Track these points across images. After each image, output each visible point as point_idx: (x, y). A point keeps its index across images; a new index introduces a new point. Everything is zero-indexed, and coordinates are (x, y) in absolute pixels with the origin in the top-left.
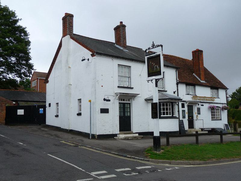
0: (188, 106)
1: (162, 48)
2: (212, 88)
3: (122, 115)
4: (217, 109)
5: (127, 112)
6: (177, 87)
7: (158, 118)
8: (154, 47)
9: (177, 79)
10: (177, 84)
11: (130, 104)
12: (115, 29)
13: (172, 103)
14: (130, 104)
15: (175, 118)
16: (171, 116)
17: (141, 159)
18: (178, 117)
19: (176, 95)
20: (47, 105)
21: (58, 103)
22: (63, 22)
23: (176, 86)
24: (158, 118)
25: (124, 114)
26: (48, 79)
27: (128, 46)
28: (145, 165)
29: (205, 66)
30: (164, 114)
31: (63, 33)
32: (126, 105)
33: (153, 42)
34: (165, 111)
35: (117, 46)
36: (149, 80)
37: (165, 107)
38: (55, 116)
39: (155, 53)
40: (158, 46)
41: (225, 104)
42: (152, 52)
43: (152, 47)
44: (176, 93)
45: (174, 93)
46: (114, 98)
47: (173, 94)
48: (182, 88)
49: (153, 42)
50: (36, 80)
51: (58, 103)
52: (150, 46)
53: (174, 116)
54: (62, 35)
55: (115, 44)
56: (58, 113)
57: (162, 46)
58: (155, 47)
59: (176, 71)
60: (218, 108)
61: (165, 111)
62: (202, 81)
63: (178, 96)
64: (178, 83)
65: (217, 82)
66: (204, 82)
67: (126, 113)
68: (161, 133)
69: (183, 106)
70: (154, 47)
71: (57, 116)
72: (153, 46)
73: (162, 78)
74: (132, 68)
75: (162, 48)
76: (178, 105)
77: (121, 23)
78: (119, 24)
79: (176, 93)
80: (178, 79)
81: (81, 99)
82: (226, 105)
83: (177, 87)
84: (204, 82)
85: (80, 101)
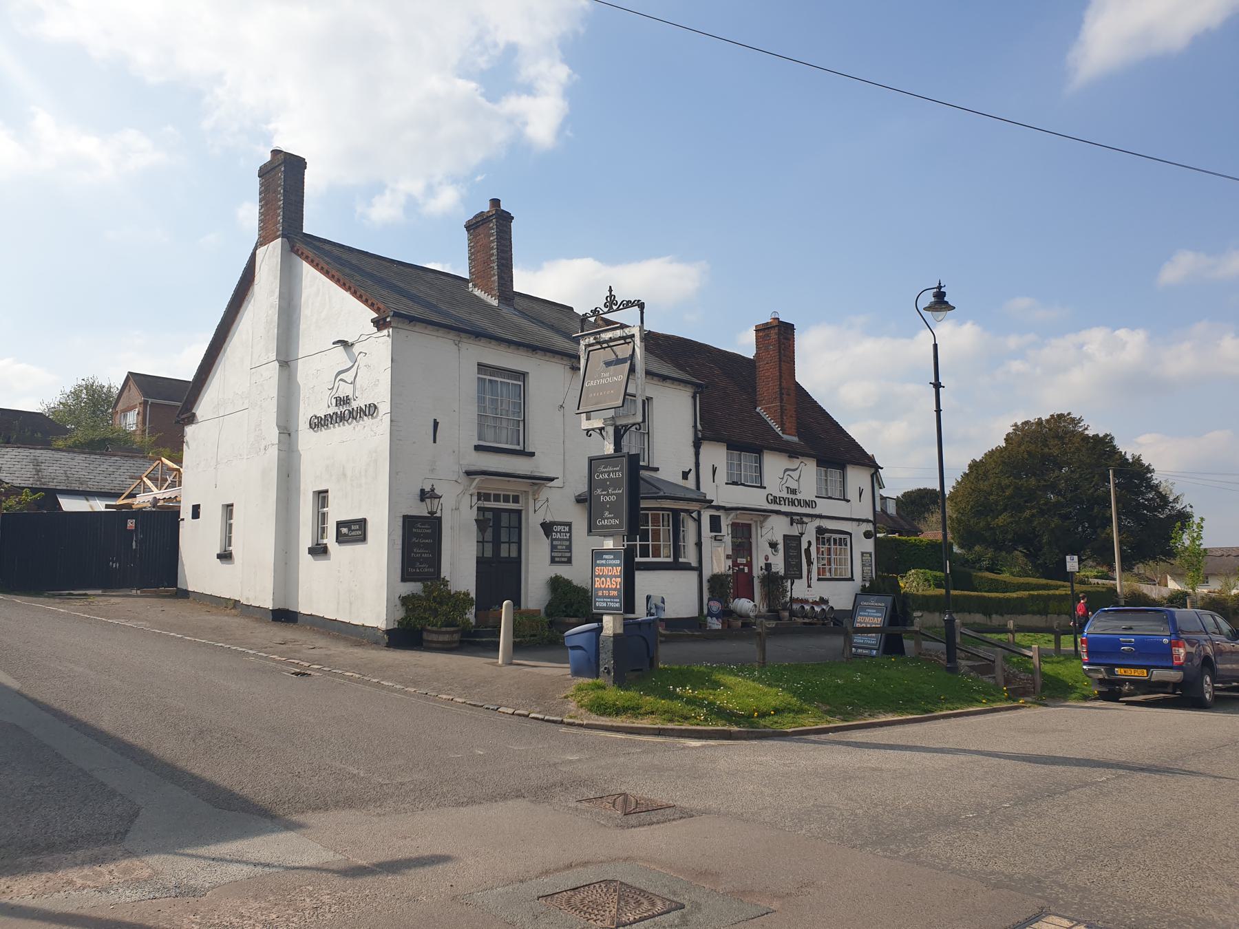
0: (735, 526)
1: (642, 313)
2: (824, 462)
3: (488, 553)
4: (835, 540)
5: (507, 545)
6: (697, 454)
7: (651, 556)
8: (615, 307)
9: (695, 426)
10: (697, 445)
11: (519, 512)
12: (472, 226)
13: (676, 513)
14: (519, 512)
15: (687, 567)
16: (670, 560)
17: (551, 718)
18: (694, 564)
19: (691, 483)
20: (186, 513)
21: (232, 505)
22: (262, 185)
23: (692, 451)
24: (651, 556)
25: (497, 549)
26: (192, 408)
27: (520, 294)
28: (1057, 588)
29: (799, 378)
30: (645, 553)
31: (261, 229)
32: (505, 517)
33: (611, 290)
34: (650, 543)
35: (477, 292)
36: (593, 430)
37: (650, 528)
38: (220, 557)
39: (623, 326)
40: (628, 304)
41: (867, 521)
42: (608, 322)
43: (605, 306)
44: (692, 476)
45: (685, 475)
46: (460, 489)
47: (678, 480)
48: (715, 455)
49: (611, 290)
50: (134, 407)
51: (232, 505)
52: (600, 303)
53: (681, 560)
54: (255, 237)
55: (470, 285)
56: (230, 545)
57: (641, 306)
58: (618, 309)
59: (694, 398)
60: (843, 536)
61: (650, 543)
62: (786, 437)
63: (698, 487)
64: (700, 439)
65: (847, 437)
66: (795, 439)
67: (504, 547)
68: (1023, 424)
69: (715, 524)
70: (615, 307)
71: (225, 556)
72: (611, 302)
73: (639, 424)
74: (532, 382)
75: (642, 313)
76: (698, 521)
77: (495, 202)
78: (486, 208)
79: (692, 476)
80: (699, 427)
81: (327, 491)
82: (871, 524)
83: (697, 454)
84: (795, 439)
85: (324, 498)
